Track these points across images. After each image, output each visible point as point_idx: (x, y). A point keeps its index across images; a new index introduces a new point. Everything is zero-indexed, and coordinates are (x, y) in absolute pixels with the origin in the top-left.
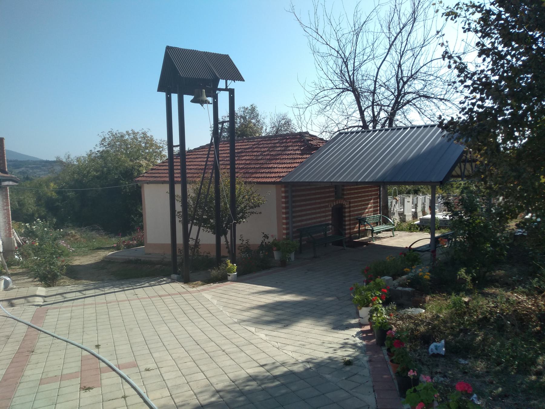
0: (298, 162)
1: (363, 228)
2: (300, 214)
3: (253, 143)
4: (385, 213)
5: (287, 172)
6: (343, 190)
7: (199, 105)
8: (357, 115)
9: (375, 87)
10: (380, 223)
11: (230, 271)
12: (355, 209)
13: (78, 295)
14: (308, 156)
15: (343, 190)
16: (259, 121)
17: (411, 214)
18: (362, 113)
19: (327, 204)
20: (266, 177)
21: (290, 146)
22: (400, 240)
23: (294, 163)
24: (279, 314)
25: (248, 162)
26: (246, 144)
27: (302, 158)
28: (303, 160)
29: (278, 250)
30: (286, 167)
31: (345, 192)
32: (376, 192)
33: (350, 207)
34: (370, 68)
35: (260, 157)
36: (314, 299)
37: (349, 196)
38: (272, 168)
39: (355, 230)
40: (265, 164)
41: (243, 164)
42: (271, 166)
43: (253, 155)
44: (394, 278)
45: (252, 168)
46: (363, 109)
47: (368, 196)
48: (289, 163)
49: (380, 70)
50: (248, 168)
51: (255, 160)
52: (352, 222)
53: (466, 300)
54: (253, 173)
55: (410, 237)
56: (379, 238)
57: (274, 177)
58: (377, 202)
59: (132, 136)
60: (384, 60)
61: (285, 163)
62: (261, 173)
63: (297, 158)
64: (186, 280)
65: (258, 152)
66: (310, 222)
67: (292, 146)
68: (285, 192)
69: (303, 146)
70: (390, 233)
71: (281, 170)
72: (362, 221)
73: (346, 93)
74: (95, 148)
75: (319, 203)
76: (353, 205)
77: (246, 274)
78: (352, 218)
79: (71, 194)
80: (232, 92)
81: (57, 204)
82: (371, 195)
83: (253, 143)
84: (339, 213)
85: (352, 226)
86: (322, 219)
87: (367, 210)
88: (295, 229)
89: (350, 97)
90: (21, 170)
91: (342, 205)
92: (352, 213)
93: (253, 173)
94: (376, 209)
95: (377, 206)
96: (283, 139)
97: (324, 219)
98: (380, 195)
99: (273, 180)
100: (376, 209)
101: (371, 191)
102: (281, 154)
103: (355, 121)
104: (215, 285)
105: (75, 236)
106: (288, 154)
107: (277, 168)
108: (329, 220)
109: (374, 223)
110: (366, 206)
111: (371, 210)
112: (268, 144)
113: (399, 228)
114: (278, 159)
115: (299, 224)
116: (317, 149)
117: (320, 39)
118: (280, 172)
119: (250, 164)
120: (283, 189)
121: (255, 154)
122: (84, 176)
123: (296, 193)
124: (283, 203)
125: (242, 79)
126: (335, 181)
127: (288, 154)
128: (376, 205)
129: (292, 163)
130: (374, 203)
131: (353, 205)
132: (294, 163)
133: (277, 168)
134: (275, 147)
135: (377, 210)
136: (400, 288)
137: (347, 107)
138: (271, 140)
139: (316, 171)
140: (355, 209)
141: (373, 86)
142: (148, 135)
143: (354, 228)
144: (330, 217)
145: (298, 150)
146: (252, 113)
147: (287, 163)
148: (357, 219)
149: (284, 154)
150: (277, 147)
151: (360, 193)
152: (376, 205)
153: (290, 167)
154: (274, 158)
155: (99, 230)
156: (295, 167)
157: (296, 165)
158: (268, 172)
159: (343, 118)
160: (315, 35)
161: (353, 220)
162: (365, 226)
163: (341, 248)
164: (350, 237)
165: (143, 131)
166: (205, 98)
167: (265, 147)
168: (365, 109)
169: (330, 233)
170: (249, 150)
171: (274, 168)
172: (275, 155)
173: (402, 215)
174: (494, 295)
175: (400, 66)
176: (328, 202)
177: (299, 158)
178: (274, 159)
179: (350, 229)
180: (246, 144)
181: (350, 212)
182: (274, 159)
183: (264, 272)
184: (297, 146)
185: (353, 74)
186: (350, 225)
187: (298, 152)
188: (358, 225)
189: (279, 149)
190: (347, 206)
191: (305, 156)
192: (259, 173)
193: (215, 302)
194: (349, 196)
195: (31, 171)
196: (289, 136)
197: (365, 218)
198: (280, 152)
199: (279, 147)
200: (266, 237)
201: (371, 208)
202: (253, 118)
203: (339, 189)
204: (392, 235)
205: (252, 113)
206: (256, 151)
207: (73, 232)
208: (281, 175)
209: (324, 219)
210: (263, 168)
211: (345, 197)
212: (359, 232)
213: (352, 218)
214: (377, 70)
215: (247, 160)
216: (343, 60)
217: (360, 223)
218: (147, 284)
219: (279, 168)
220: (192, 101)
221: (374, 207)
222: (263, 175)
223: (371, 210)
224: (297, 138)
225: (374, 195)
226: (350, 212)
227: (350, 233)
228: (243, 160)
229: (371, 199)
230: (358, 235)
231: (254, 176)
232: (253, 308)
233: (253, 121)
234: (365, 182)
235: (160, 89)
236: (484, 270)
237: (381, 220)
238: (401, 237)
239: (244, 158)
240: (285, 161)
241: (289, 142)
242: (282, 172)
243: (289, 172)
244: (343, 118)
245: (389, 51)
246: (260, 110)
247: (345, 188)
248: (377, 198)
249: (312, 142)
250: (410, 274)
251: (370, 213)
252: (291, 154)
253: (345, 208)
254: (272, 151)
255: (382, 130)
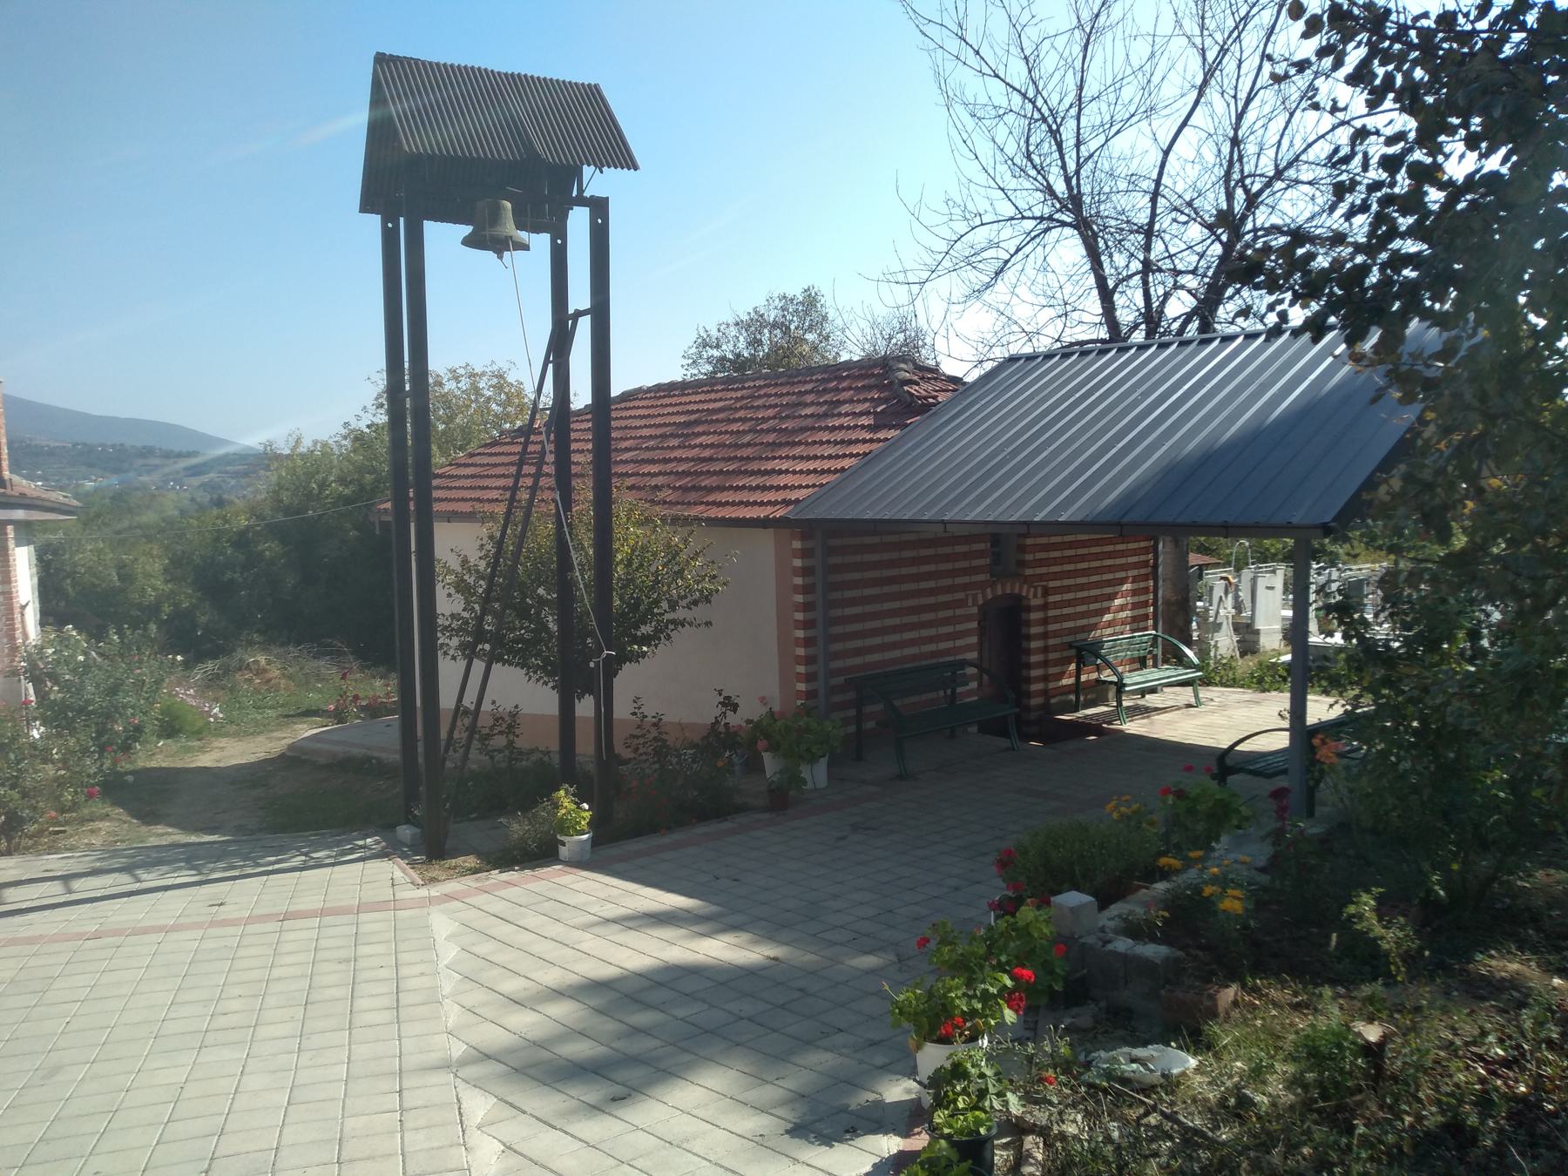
0: (858, 455)
1: (1094, 676)
2: (858, 627)
3: (739, 394)
4: (1176, 622)
5: (814, 486)
6: (1022, 549)
7: (490, 255)
8: (1094, 305)
9: (1153, 215)
10: (1155, 658)
11: (565, 827)
12: (1066, 611)
13: (54, 890)
14: (892, 434)
15: (1022, 549)
16: (827, 338)
17: (1278, 626)
18: (1106, 296)
19: (960, 596)
20: (747, 504)
21: (845, 402)
22: (1217, 719)
23: (844, 456)
24: (637, 1031)
25: (707, 453)
26: (719, 395)
27: (871, 441)
28: (874, 446)
29: (774, 748)
30: (815, 471)
31: (1029, 557)
32: (1143, 558)
33: (1045, 607)
34: (1134, 150)
35: (747, 439)
36: (810, 957)
37: (1043, 570)
38: (773, 471)
39: (1065, 682)
40: (754, 459)
41: (692, 459)
42: (769, 466)
43: (726, 432)
44: (1105, 900)
45: (715, 473)
46: (1111, 283)
47: (1111, 569)
48: (830, 457)
49: (1171, 155)
50: (702, 473)
51: (730, 446)
52: (1052, 656)
53: (1373, 1033)
54: (710, 490)
55: (1256, 708)
56: (1146, 711)
57: (770, 503)
58: (1146, 591)
59: (464, 384)
60: (1184, 124)
61: (816, 457)
62: (738, 488)
63: (857, 441)
64: (433, 850)
65: (743, 420)
66: (896, 654)
67: (851, 401)
68: (805, 554)
69: (886, 400)
70: (1186, 694)
71: (797, 481)
72: (1087, 653)
73: (1055, 233)
74: (358, 417)
75: (932, 592)
76: (1057, 598)
77: (620, 842)
78: (1051, 642)
79: (270, 548)
80: (599, 207)
81: (228, 575)
82: (1123, 568)
83: (739, 394)
84: (1007, 625)
85: (1052, 670)
86: (943, 646)
87: (1107, 617)
88: (840, 680)
89: (1068, 248)
90: (206, 478)
91: (1018, 598)
92: (1051, 627)
93: (710, 490)
94: (1141, 611)
95: (1145, 604)
96: (830, 380)
97: (949, 644)
98: (1155, 566)
99: (761, 513)
100: (1141, 611)
101: (1122, 554)
102: (813, 428)
103: (1087, 325)
104: (506, 876)
105: (265, 671)
106: (834, 429)
107: (787, 472)
108: (969, 648)
109: (1132, 661)
110: (1105, 604)
111: (1123, 615)
112: (782, 395)
113: (1211, 676)
114: (800, 443)
115: (858, 661)
116: (926, 408)
117: (972, 60)
118: (793, 488)
119: (710, 459)
120: (797, 544)
121: (735, 427)
122: (309, 496)
123: (840, 558)
124: (796, 589)
125: (628, 162)
126: (957, 518)
127: (834, 429)
128: (1142, 598)
129: (837, 457)
130: (1134, 593)
131: (1057, 598)
132: (844, 456)
133: (787, 472)
134: (800, 404)
135: (1146, 617)
136: (1122, 945)
137: (1063, 279)
138: (794, 384)
139: (928, 483)
140: (1066, 611)
141: (1148, 211)
142: (511, 378)
143: (1061, 676)
144: (974, 640)
145: (867, 413)
146: (806, 313)
147: (823, 457)
148: (1070, 646)
149: (821, 429)
150: (807, 405)
151: (1082, 558)
152: (1142, 598)
153: (829, 471)
154: (788, 439)
155: (339, 653)
156: (843, 469)
157: (846, 463)
158: (758, 487)
159: (1051, 312)
160: (953, 45)
161: (1056, 648)
162: (1099, 669)
163: (1003, 742)
164: (1046, 706)
165: (495, 368)
166: (509, 228)
167: (770, 406)
168: (1116, 286)
169: (970, 690)
170: (721, 416)
171: (780, 472)
172: (794, 431)
173: (1247, 635)
174: (1511, 996)
175: (1235, 142)
176: (965, 587)
177: (865, 441)
178: (788, 443)
179: (1046, 678)
180: (719, 395)
181: (1045, 621)
182: (788, 443)
183: (701, 829)
184: (866, 400)
185: (1077, 173)
186: (1046, 664)
187: (865, 421)
188: (1073, 667)
189: (809, 411)
190: (1034, 602)
191: (881, 435)
192: (731, 487)
193: (449, 953)
194: (1043, 570)
195: (233, 482)
196: (849, 369)
197: (1099, 644)
198: (809, 422)
199: (812, 404)
200: (729, 704)
201: (1122, 608)
202: (810, 329)
203: (1006, 546)
204: (1193, 701)
205: (806, 313)
206: (740, 419)
207: (262, 659)
208: (793, 495)
209: (949, 644)
210: (746, 472)
211: (1029, 572)
212: (1077, 687)
213: (1051, 642)
214: (1161, 155)
215: (707, 446)
216: (1050, 127)
217: (1081, 663)
218: (298, 861)
219: (794, 472)
220: (468, 242)
221: (1135, 606)
222: (738, 496)
223: (1123, 615)
224: (873, 375)
225: (1136, 566)
226: (1045, 621)
227: (1045, 693)
228: (695, 446)
229: (1122, 581)
230: (1072, 697)
231: (711, 498)
232: (558, 994)
233: (810, 337)
234: (1058, 523)
235: (367, 206)
236: (1484, 864)
237: (1159, 651)
238: (1223, 707)
239: (698, 441)
240: (818, 451)
241: (844, 389)
242: (800, 487)
243: (822, 485)
244: (1051, 312)
245: (1200, 95)
246: (830, 304)
247: (1029, 541)
248: (1145, 578)
249: (913, 389)
250: (1180, 880)
251: (1118, 627)
252: (841, 427)
253: (1029, 609)
254: (787, 417)
255: (1149, 346)
